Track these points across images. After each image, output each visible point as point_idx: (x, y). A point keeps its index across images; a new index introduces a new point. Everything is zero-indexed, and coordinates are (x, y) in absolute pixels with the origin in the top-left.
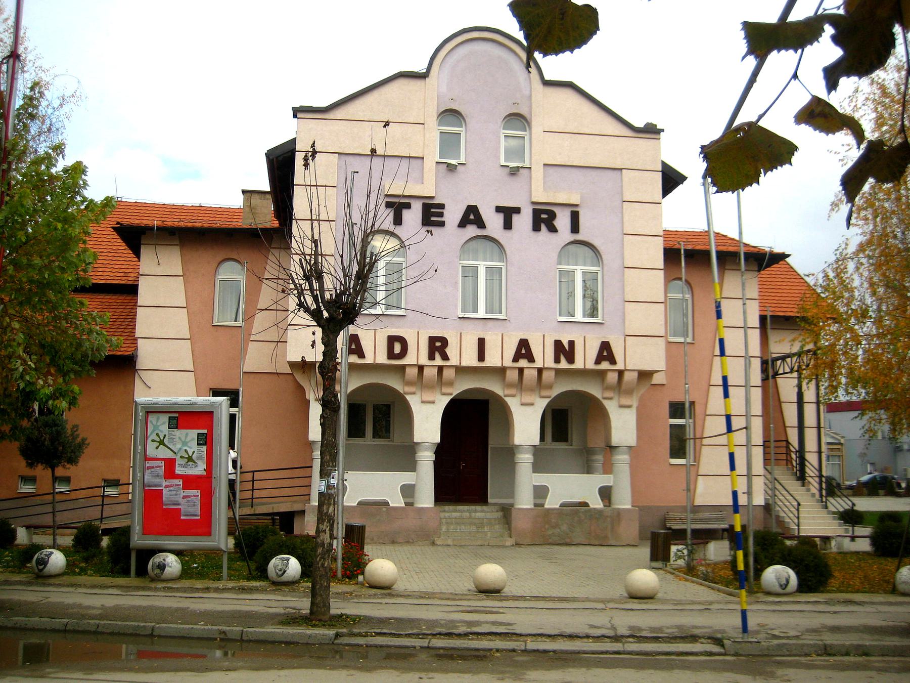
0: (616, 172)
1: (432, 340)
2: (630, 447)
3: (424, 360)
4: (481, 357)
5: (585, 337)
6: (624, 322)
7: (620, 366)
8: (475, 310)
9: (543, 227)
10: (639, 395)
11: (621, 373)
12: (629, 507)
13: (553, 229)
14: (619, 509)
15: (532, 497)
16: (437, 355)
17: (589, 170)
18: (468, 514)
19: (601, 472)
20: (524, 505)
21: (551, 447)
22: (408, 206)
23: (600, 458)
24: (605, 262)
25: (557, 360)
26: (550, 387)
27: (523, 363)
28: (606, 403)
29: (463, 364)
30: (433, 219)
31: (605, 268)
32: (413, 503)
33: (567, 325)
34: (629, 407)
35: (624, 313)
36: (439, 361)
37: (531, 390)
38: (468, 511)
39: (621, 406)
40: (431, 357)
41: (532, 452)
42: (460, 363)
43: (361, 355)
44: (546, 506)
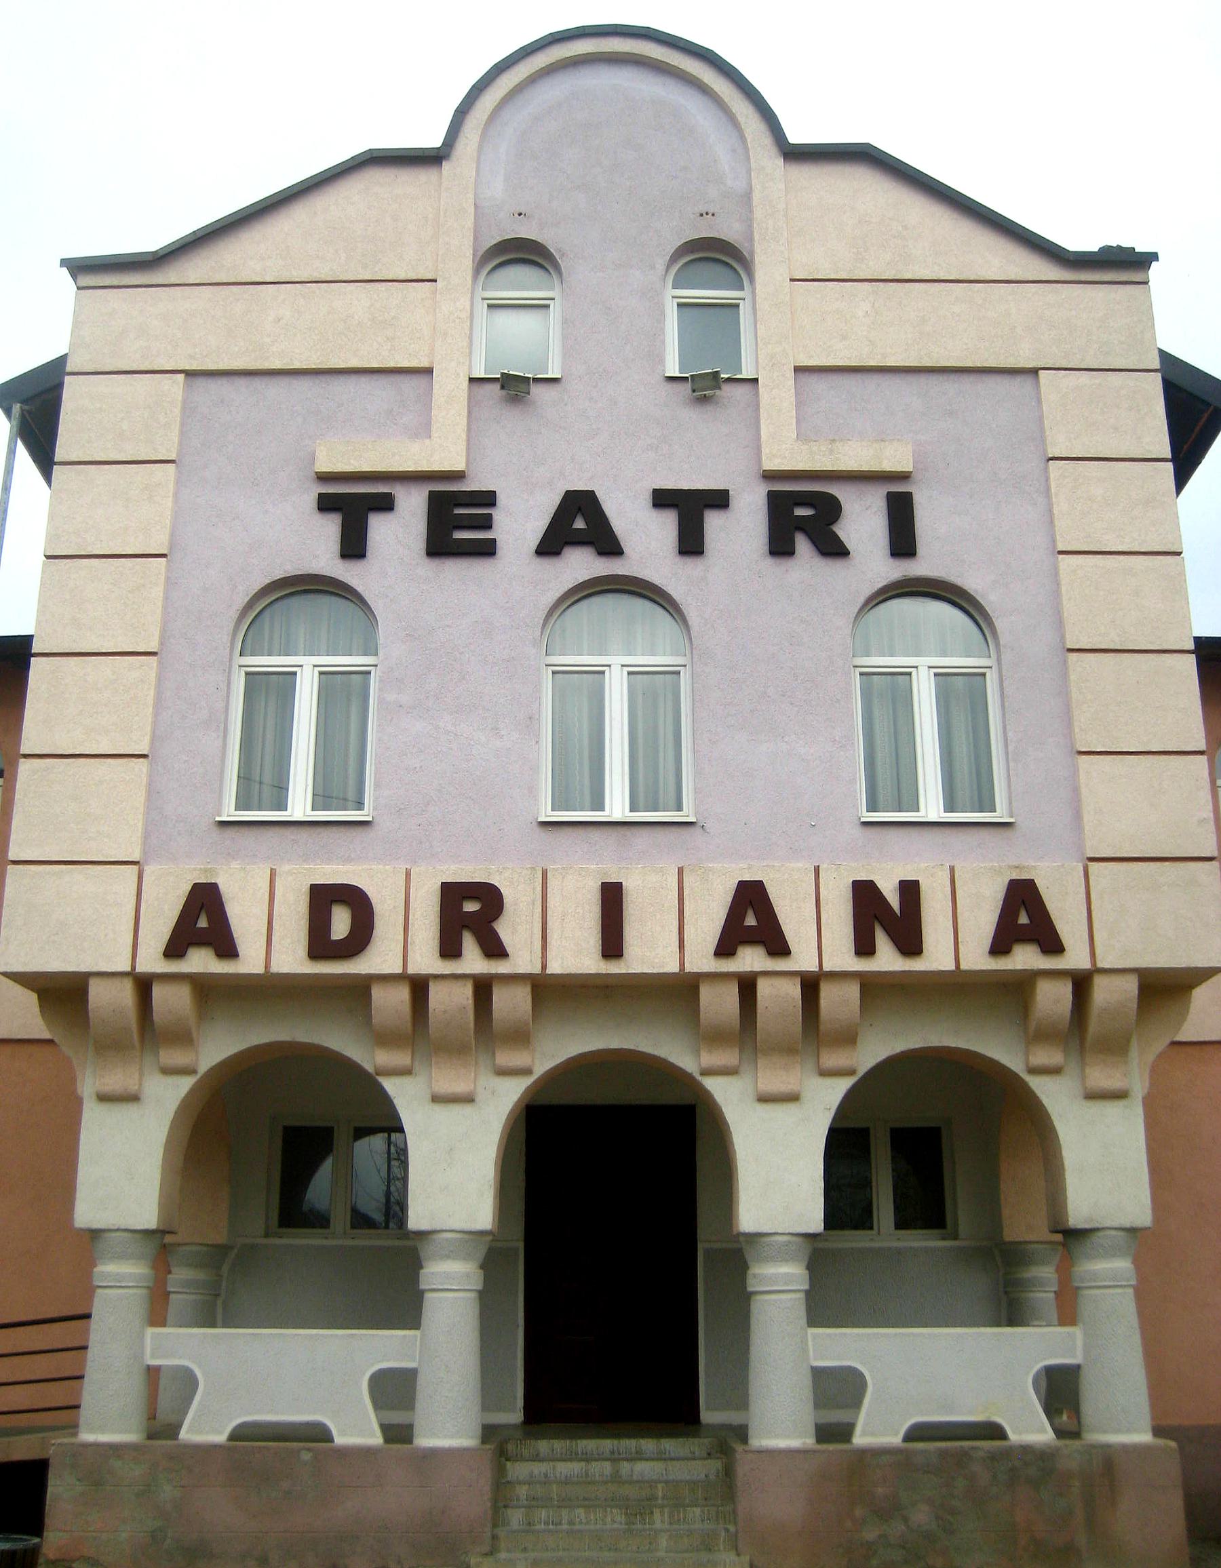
0: (1018, 380)
1: (452, 894)
2: (1132, 1231)
3: (425, 959)
4: (612, 945)
5: (952, 870)
6: (1078, 816)
7: (1076, 957)
8: (599, 805)
9: (802, 544)
10: (1151, 1057)
11: (1081, 983)
12: (1144, 1437)
13: (833, 549)
14: (1108, 1446)
15: (811, 1404)
16: (469, 944)
17: (934, 379)
18: (607, 1467)
19: (1054, 1317)
20: (777, 1436)
21: (895, 1244)
22: (385, 504)
23: (1045, 1273)
24: (1002, 641)
25: (864, 947)
26: (848, 1038)
27: (751, 959)
28: (1041, 1086)
29: (555, 968)
30: (459, 535)
31: (1007, 657)
32: (410, 1427)
33: (893, 833)
34: (1119, 1095)
35: (1076, 790)
36: (473, 961)
37: (787, 1050)
38: (614, 1458)
39: (1094, 1096)
40: (449, 949)
41: (806, 1259)
42: (544, 967)
43: (226, 948)
44: (860, 1439)
